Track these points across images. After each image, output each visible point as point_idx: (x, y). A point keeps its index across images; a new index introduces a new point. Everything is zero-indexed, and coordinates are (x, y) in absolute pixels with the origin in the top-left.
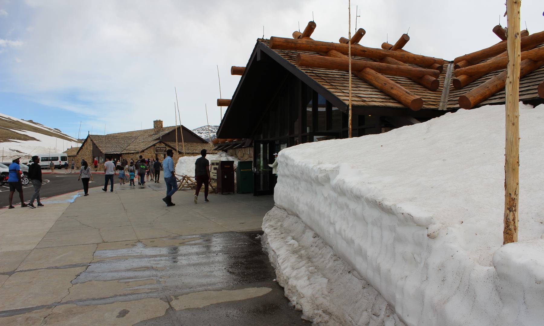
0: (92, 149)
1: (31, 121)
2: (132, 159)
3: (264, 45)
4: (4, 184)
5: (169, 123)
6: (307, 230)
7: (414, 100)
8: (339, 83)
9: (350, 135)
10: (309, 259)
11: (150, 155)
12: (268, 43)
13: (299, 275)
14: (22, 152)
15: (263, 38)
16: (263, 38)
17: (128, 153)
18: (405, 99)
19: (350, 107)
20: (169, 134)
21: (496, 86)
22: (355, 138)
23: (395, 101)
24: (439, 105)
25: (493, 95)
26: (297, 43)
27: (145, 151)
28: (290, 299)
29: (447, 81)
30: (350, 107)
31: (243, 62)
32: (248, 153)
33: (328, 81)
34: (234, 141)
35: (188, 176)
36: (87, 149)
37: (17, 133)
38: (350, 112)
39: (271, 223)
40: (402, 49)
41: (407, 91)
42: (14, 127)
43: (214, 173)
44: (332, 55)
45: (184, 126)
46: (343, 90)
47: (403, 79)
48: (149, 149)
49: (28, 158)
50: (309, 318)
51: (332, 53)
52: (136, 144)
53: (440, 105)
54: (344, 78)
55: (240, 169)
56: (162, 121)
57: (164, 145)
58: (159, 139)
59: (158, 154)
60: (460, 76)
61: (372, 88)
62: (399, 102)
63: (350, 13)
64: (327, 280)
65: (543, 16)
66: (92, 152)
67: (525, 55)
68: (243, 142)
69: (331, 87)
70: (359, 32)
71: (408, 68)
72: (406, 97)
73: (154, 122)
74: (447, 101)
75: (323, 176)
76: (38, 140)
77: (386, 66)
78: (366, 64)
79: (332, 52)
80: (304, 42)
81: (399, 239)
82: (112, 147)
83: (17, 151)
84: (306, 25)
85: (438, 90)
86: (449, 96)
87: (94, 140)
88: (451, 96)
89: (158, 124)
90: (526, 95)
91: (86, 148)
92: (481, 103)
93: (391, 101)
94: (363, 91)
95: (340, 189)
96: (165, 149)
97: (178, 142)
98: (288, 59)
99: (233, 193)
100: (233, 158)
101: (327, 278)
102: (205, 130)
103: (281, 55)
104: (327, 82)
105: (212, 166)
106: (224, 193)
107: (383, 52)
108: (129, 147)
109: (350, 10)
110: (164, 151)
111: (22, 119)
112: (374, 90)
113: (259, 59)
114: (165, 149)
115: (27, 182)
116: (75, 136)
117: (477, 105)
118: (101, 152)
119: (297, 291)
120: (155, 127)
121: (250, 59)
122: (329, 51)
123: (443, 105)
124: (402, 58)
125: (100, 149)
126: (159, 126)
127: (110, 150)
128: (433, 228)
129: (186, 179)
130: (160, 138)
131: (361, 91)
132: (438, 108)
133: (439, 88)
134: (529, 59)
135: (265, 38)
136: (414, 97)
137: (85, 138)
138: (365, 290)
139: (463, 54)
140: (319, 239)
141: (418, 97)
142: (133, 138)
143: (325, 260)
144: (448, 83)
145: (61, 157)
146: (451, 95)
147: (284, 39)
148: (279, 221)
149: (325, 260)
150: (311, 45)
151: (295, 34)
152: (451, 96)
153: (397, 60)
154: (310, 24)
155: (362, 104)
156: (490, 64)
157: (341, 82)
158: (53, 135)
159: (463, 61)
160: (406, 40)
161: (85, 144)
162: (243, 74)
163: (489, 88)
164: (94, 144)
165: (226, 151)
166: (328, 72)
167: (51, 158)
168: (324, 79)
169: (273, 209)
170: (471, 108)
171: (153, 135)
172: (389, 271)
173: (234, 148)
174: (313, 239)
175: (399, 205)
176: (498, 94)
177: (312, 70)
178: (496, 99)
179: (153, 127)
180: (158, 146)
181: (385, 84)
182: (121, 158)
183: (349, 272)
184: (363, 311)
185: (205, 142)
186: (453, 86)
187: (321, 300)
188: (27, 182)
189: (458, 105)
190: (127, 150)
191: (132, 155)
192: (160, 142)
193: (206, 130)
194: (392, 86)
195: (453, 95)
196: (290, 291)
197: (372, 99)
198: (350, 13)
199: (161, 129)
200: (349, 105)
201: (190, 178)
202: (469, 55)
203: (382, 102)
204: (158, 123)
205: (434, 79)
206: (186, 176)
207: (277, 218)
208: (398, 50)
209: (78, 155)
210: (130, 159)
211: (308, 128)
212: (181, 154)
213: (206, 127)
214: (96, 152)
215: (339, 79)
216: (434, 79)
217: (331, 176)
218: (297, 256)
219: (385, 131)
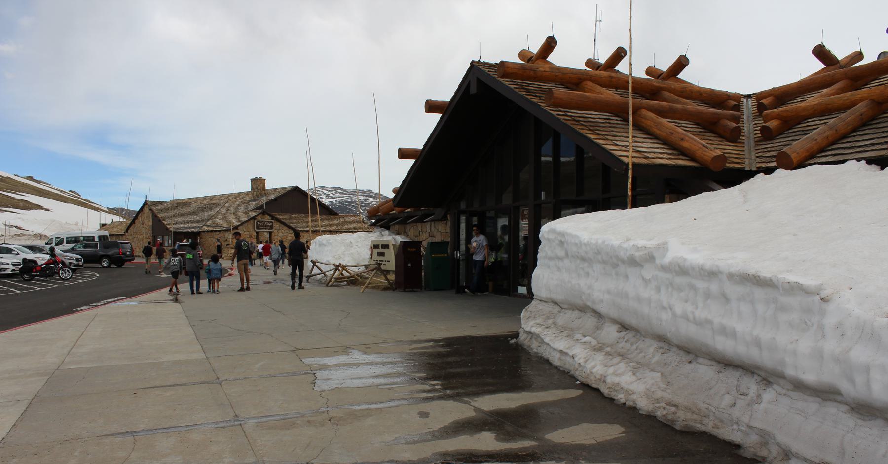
0: (151, 223)
1: (30, 178)
2: (218, 240)
3: (484, 71)
4: (34, 277)
5: (276, 181)
6: (606, 324)
7: (716, 156)
8: (606, 131)
9: (629, 205)
10: (622, 356)
11: (247, 233)
12: (496, 72)
13: (619, 372)
14: (24, 229)
15: (479, 61)
16: (479, 61)
17: (212, 231)
18: (702, 155)
19: (630, 166)
20: (276, 200)
21: (827, 138)
22: (640, 210)
23: (687, 158)
24: (744, 163)
25: (823, 150)
26: (538, 70)
27: (239, 228)
28: (614, 398)
29: (750, 127)
30: (630, 166)
31: (446, 94)
32: (428, 230)
33: (591, 128)
34: (407, 211)
35: (344, 263)
36: (143, 224)
37: (12, 198)
38: (630, 173)
39: (538, 321)
40: (678, 77)
41: (702, 142)
42: (5, 187)
44: (587, 88)
46: (615, 142)
47: (688, 124)
48: (246, 224)
49: (39, 238)
50: (648, 412)
51: (586, 86)
52: (224, 216)
53: (746, 163)
54: (610, 123)
56: (265, 180)
57: (269, 217)
58: (261, 207)
60: (770, 122)
61: (651, 139)
62: (692, 159)
63: (631, 36)
64: (660, 374)
65: (887, 34)
66: (151, 229)
67: (866, 95)
68: (423, 213)
69: (598, 137)
70: (617, 53)
71: (697, 110)
72: (704, 153)
73: (252, 180)
74: (753, 157)
75: (643, 254)
76: (47, 210)
77: (668, 107)
78: (641, 104)
79: (586, 84)
80: (547, 70)
81: (784, 309)
82: (184, 221)
83: (18, 228)
84: (542, 41)
85: (739, 140)
86: (757, 150)
87: (154, 209)
88: (759, 149)
89: (258, 183)
90: (869, 152)
91: (141, 222)
92: (806, 161)
93: (681, 157)
94: (641, 143)
95: (679, 267)
96: (271, 224)
97: (311, 213)
98: (526, 94)
99: (419, 290)
100: (402, 238)
101: (658, 372)
102: (317, 194)
103: (515, 88)
104: (590, 130)
105: (374, 250)
106: (406, 290)
107: (657, 84)
108: (211, 221)
109: (631, 33)
110: (269, 228)
111: (15, 175)
112: (655, 142)
113: (473, 90)
114: (271, 224)
115: (69, 275)
116: (105, 204)
117: (801, 165)
118: (167, 229)
119: (622, 388)
120: (252, 188)
121: (457, 90)
122: (581, 82)
123: (749, 163)
124: (682, 92)
125: (166, 223)
126: (259, 187)
127: (182, 226)
128: (824, 294)
129: (340, 268)
130: (263, 206)
131: (638, 142)
132: (744, 168)
133: (741, 138)
134: (870, 100)
135: (482, 60)
136: (715, 152)
137: (138, 209)
138: (721, 375)
140: (627, 334)
141: (719, 152)
142: (217, 206)
143: (647, 354)
144: (749, 130)
146: (759, 148)
147: (519, 65)
148: (548, 318)
149: (647, 354)
150: (557, 74)
151: (522, 54)
152: (759, 149)
153: (677, 96)
154: (549, 40)
155: (645, 162)
156: (815, 105)
157: (607, 130)
158: (69, 202)
159: (770, 98)
161: (140, 215)
162: (444, 112)
163: (818, 141)
164: (155, 217)
165: (388, 228)
166: (586, 113)
167: (82, 239)
168: (585, 126)
169: (534, 302)
170: (794, 167)
171: (250, 201)
172: (774, 339)
173: (408, 222)
174: (617, 334)
175: (780, 276)
176: (830, 148)
177: (565, 112)
178: (827, 156)
179: (249, 189)
180: (259, 219)
181: (671, 133)
182: (199, 238)
183: (690, 362)
184: (723, 395)
185: (333, 213)
186: (760, 135)
187: (659, 394)
188: (69, 275)
189: (775, 162)
190: (210, 226)
191: (218, 233)
192: (263, 213)
193: (319, 194)
194: (682, 137)
195: (537, 85)
196: (612, 390)
197: (656, 155)
198: (631, 36)
199: (264, 192)
200: (628, 163)
202: (779, 88)
203: (670, 158)
204: (259, 183)
205: (734, 125)
206: (340, 264)
207: (543, 315)
208: (671, 78)
209: (127, 234)
210: (214, 240)
211: (543, 192)
212: (316, 233)
214: (159, 227)
215: (601, 125)
216: (734, 125)
217: (656, 254)
218: (604, 353)
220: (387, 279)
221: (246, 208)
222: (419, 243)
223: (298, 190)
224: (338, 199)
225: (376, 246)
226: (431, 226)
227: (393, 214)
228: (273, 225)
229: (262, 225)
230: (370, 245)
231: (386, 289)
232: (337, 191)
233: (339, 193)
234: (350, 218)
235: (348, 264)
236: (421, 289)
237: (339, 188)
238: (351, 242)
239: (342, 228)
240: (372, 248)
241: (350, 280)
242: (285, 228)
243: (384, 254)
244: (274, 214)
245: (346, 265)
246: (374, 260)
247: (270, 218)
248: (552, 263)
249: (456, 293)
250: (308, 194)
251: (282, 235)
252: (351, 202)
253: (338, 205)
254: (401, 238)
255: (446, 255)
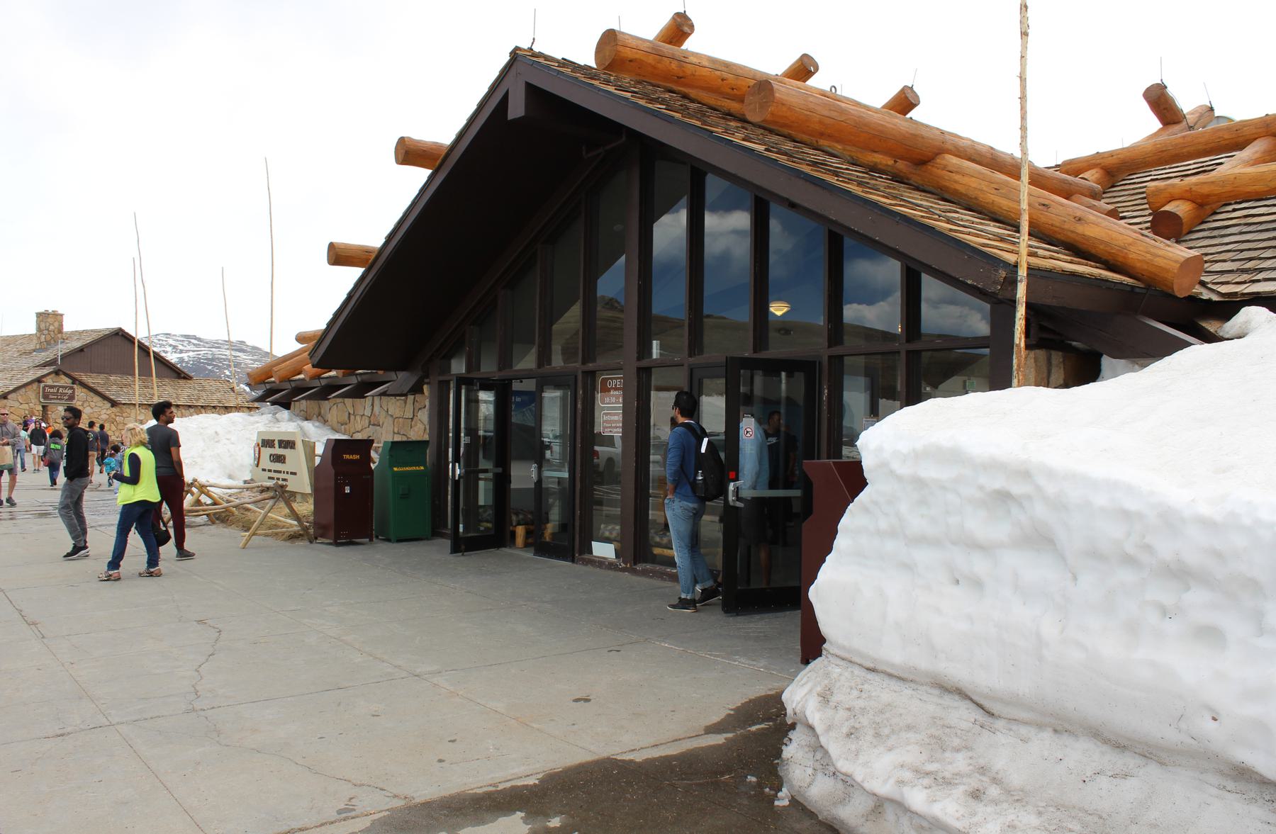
11: (26, 406)
19: (1022, 272)
26: (687, 60)
27: (9, 397)
30: (1022, 272)
32: (368, 412)
43: (270, 471)
45: (126, 331)
48: (23, 390)
55: (391, 467)
56: (62, 315)
59: (50, 406)
73: (39, 315)
89: (49, 321)
96: (70, 391)
113: (517, 110)
114: (70, 391)
120: (39, 329)
129: (194, 490)
135: (536, 49)
139: (1092, 152)
145: (278, 440)
150: (725, 75)
160: (912, 103)
165: (287, 406)
180: (49, 381)
185: (182, 376)
192: (57, 373)
193: (161, 345)
199: (59, 335)
201: (208, 488)
206: (195, 480)
211: (655, 343)
213: (159, 337)
219: (149, 376)
220: (294, 515)
221: (26, 362)
222: (367, 444)
223: (122, 335)
224: (191, 354)
225: (267, 443)
226: (373, 405)
227: (299, 380)
228: (74, 392)
229: (53, 394)
230: (254, 439)
231: (293, 537)
232: (190, 342)
233: (194, 344)
234: (210, 385)
235: (212, 481)
236: (371, 540)
237: (195, 338)
238: (216, 432)
239: (197, 400)
240: (258, 445)
241: (215, 514)
242: (97, 399)
243: (285, 458)
244: (76, 374)
245: (208, 484)
246: (264, 470)
247: (70, 381)
248: (923, 556)
249: (451, 553)
250: (134, 338)
251: (91, 411)
252: (213, 360)
253: (191, 363)
254: (313, 425)
255: (422, 468)
